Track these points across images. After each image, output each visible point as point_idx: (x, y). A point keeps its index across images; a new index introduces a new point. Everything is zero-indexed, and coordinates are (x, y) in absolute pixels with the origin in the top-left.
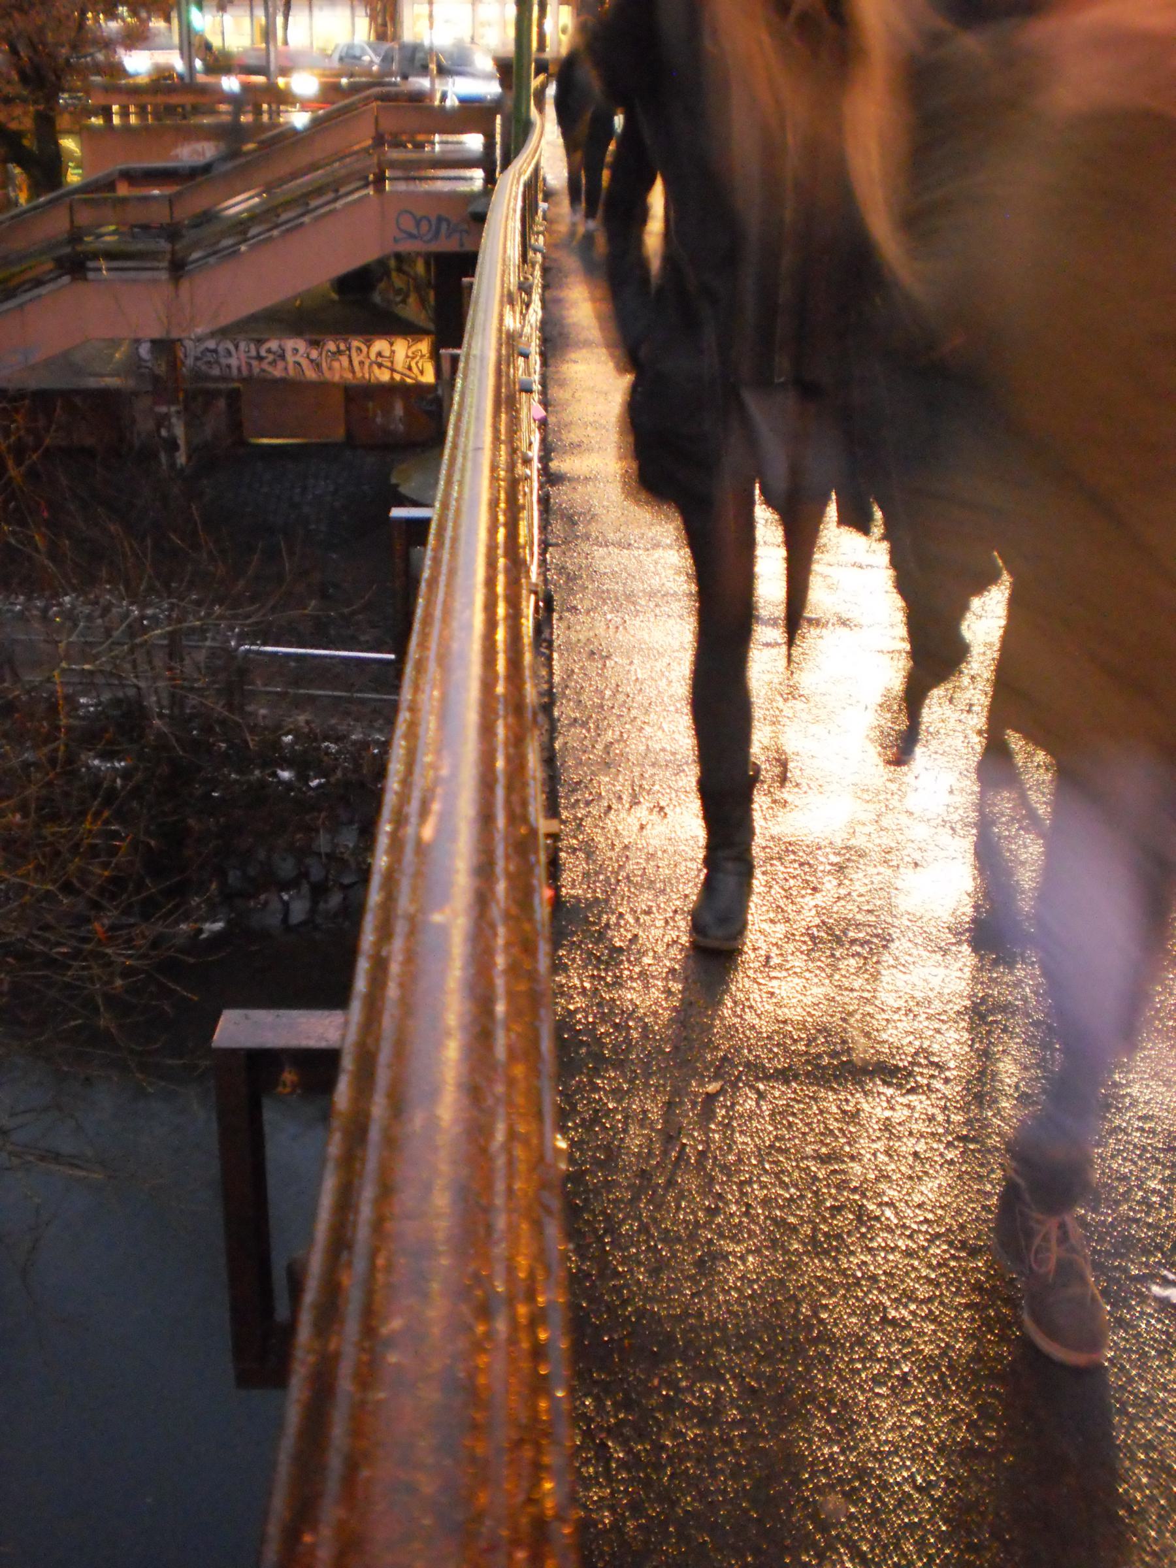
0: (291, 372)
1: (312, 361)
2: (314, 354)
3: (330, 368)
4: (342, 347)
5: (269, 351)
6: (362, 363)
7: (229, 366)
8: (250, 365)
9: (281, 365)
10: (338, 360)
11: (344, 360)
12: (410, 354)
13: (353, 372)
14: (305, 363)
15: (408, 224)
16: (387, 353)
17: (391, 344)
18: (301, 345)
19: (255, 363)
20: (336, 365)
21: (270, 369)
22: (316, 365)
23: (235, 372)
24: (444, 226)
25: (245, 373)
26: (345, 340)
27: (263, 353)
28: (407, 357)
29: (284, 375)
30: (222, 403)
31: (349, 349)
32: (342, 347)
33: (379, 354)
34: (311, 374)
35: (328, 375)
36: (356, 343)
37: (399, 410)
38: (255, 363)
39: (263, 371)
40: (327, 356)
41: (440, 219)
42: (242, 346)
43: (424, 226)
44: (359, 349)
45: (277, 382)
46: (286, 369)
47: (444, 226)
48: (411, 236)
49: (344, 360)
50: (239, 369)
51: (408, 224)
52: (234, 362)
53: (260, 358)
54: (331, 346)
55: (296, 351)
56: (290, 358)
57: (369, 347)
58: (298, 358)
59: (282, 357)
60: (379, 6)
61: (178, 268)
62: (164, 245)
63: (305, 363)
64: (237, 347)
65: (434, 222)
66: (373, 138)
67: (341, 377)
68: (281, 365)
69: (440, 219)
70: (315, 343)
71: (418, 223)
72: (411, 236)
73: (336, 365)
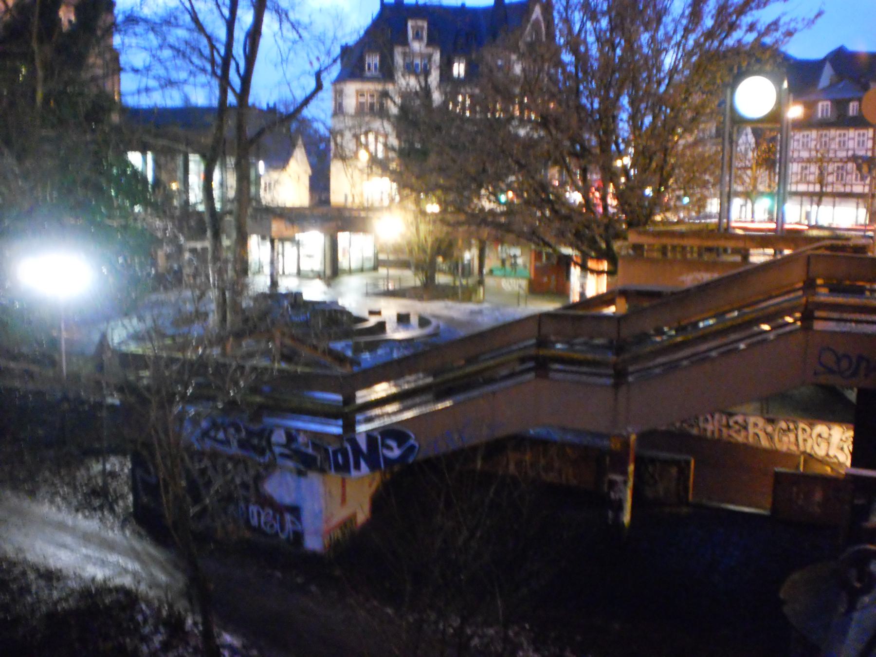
0: (751, 439)
1: (767, 434)
2: (769, 429)
3: (780, 441)
4: (792, 426)
5: (736, 423)
6: (805, 440)
7: (705, 430)
8: (720, 431)
9: (743, 433)
10: (787, 436)
11: (792, 437)
12: (844, 439)
13: (797, 445)
14: (762, 435)
15: (829, 359)
16: (825, 435)
17: (830, 429)
18: (761, 422)
19: (725, 430)
20: (785, 439)
21: (734, 435)
22: (770, 436)
23: (709, 434)
24: (864, 365)
25: (716, 435)
26: (794, 422)
27: (731, 423)
28: (841, 440)
29: (745, 441)
30: (674, 471)
31: (796, 429)
32: (792, 426)
33: (820, 436)
34: (765, 443)
35: (778, 446)
36: (802, 425)
37: (818, 496)
38: (725, 430)
39: (730, 436)
40: (779, 432)
41: (860, 358)
42: (717, 416)
43: (844, 364)
44: (804, 430)
45: (737, 445)
46: (747, 437)
47: (864, 365)
48: (831, 371)
49: (792, 437)
50: (713, 432)
51: (829, 359)
52: (710, 427)
53: (728, 426)
54: (783, 425)
55: (756, 425)
56: (751, 430)
57: (812, 429)
58: (757, 431)
59: (745, 428)
60: (870, 234)
61: (620, 376)
62: (611, 357)
63: (762, 435)
64: (713, 417)
65: (854, 360)
66: (804, 282)
67: (789, 449)
68: (743, 433)
69: (860, 358)
70: (771, 421)
71: (839, 360)
72: (831, 371)
73: (785, 439)
